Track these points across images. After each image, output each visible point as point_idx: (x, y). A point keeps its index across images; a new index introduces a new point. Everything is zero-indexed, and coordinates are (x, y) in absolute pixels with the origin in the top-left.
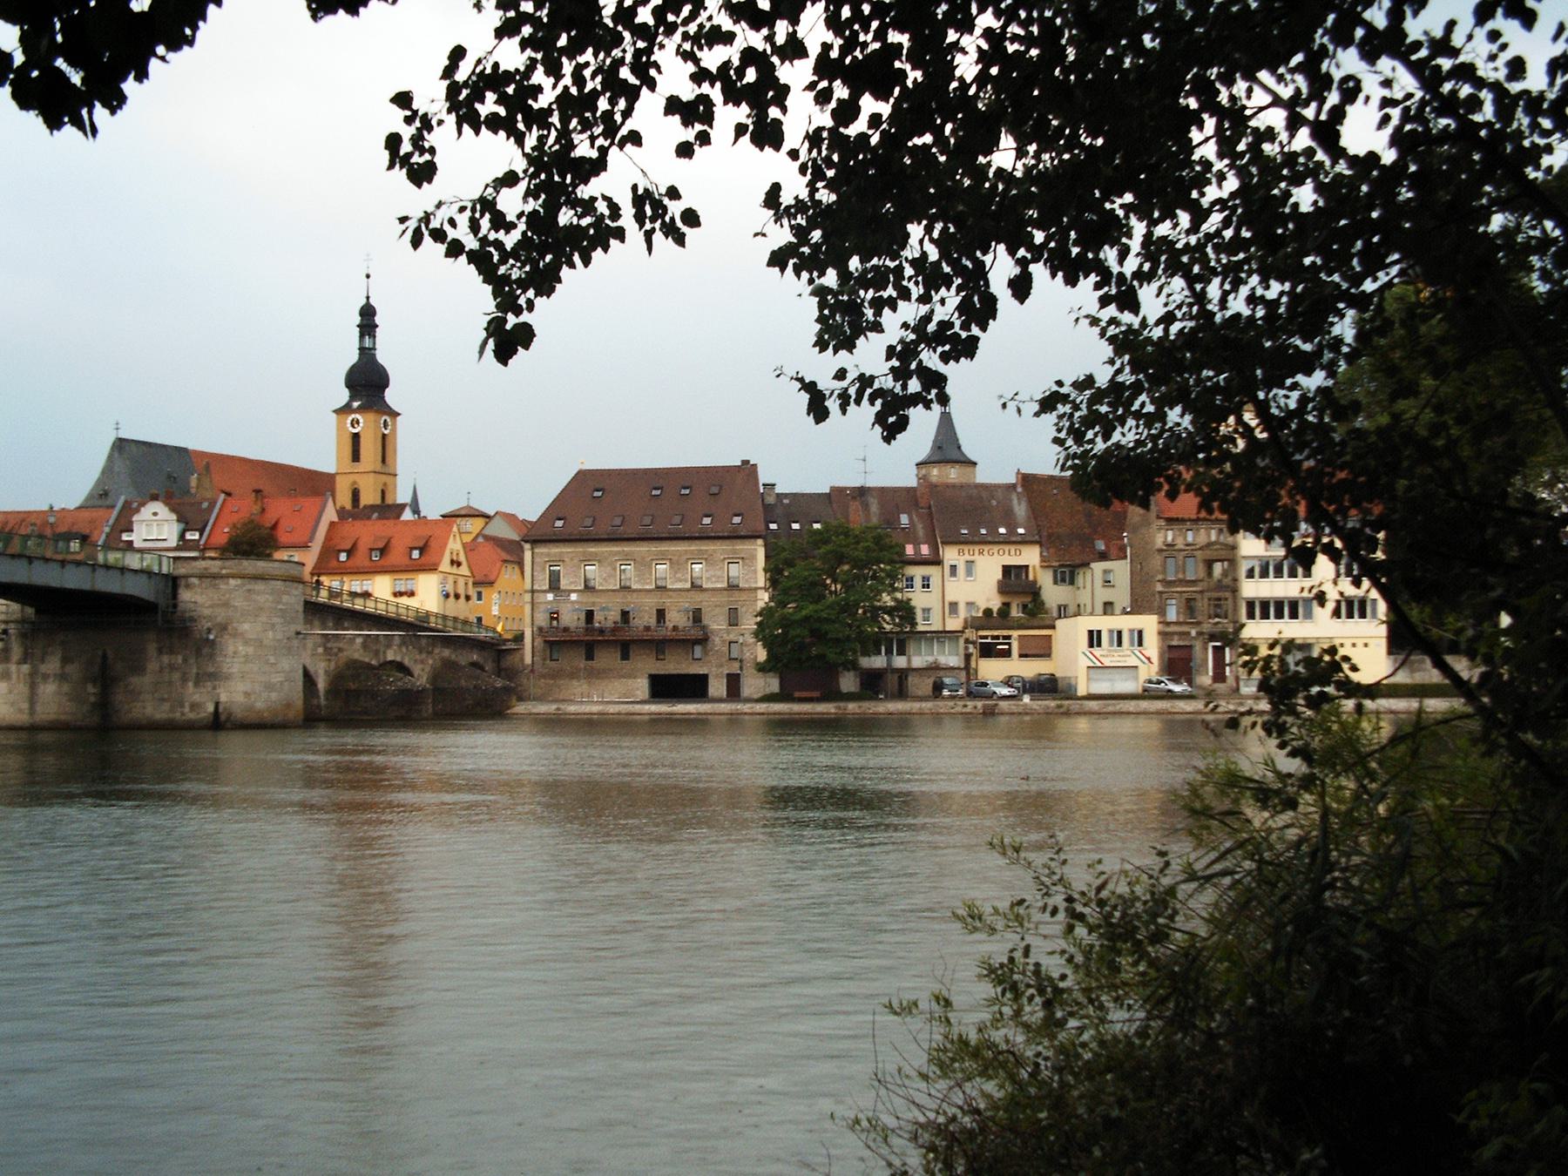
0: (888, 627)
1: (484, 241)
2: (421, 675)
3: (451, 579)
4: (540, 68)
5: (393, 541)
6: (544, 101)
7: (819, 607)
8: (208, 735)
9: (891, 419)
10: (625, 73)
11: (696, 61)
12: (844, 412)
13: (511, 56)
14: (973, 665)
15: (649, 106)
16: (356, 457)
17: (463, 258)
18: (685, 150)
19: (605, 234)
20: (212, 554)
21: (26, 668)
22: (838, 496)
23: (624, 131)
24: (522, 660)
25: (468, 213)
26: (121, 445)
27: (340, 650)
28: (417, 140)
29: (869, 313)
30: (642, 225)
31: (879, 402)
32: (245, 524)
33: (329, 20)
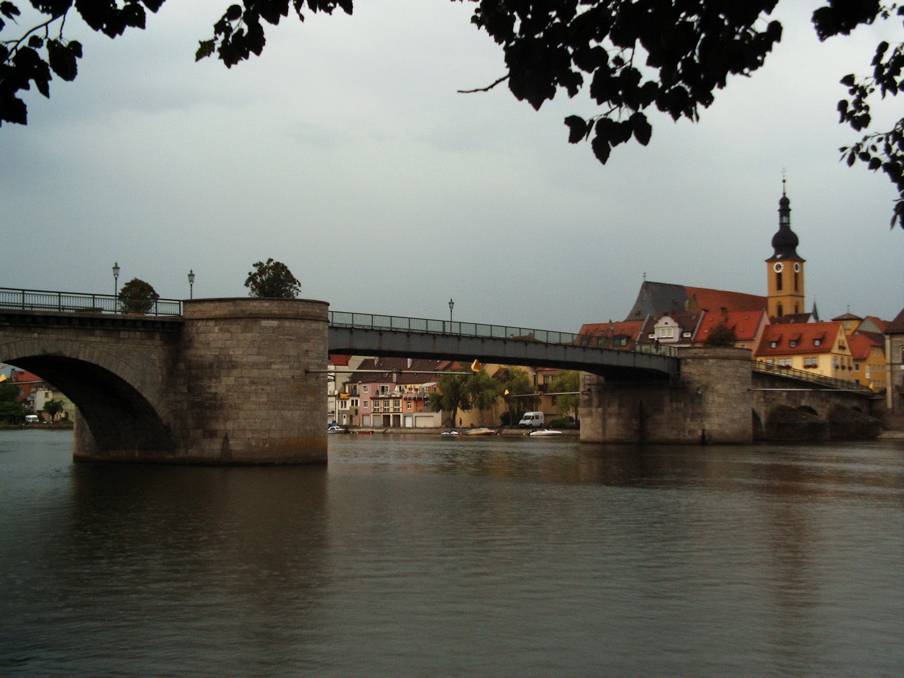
1: (894, 157)
2: (823, 413)
3: (839, 357)
16: (779, 286)
17: (881, 169)
20: (698, 345)
21: (600, 410)
24: (886, 405)
25: (884, 142)
26: (647, 285)
27: (774, 399)
28: (858, 104)
33: (831, 40)
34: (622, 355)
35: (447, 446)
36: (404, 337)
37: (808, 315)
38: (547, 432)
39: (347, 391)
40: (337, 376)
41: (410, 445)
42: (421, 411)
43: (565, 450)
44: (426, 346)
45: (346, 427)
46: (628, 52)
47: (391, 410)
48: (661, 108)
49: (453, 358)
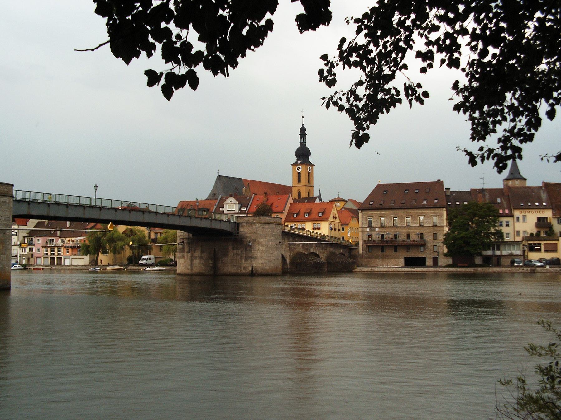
0: (493, 240)
1: (351, 105)
2: (323, 256)
3: (333, 223)
4: (372, 44)
5: (313, 210)
6: (373, 55)
7: (467, 233)
8: (249, 278)
9: (501, 165)
10: (401, 44)
11: (427, 38)
12: (483, 163)
13: (361, 40)
14: (526, 254)
15: (410, 56)
16: (299, 181)
17: (344, 111)
18: (423, 70)
19: (394, 101)
20: (250, 215)
21: (189, 254)
22: (473, 192)
23: (401, 64)
24: (358, 252)
25: (346, 96)
26: (220, 178)
27: (294, 248)
28: (329, 71)
29: (491, 126)
30: (408, 98)
31: (496, 159)
32: (261, 205)
33: (306, 33)
34: (203, 220)
35: (91, 277)
36: (64, 207)
37: (316, 198)
38: (156, 268)
39: (26, 242)
40: (18, 233)
41: (67, 277)
42: (75, 255)
43: (167, 279)
44: (79, 214)
45: (25, 265)
46: (185, 31)
47: (56, 254)
48: (206, 68)
49: (97, 221)
